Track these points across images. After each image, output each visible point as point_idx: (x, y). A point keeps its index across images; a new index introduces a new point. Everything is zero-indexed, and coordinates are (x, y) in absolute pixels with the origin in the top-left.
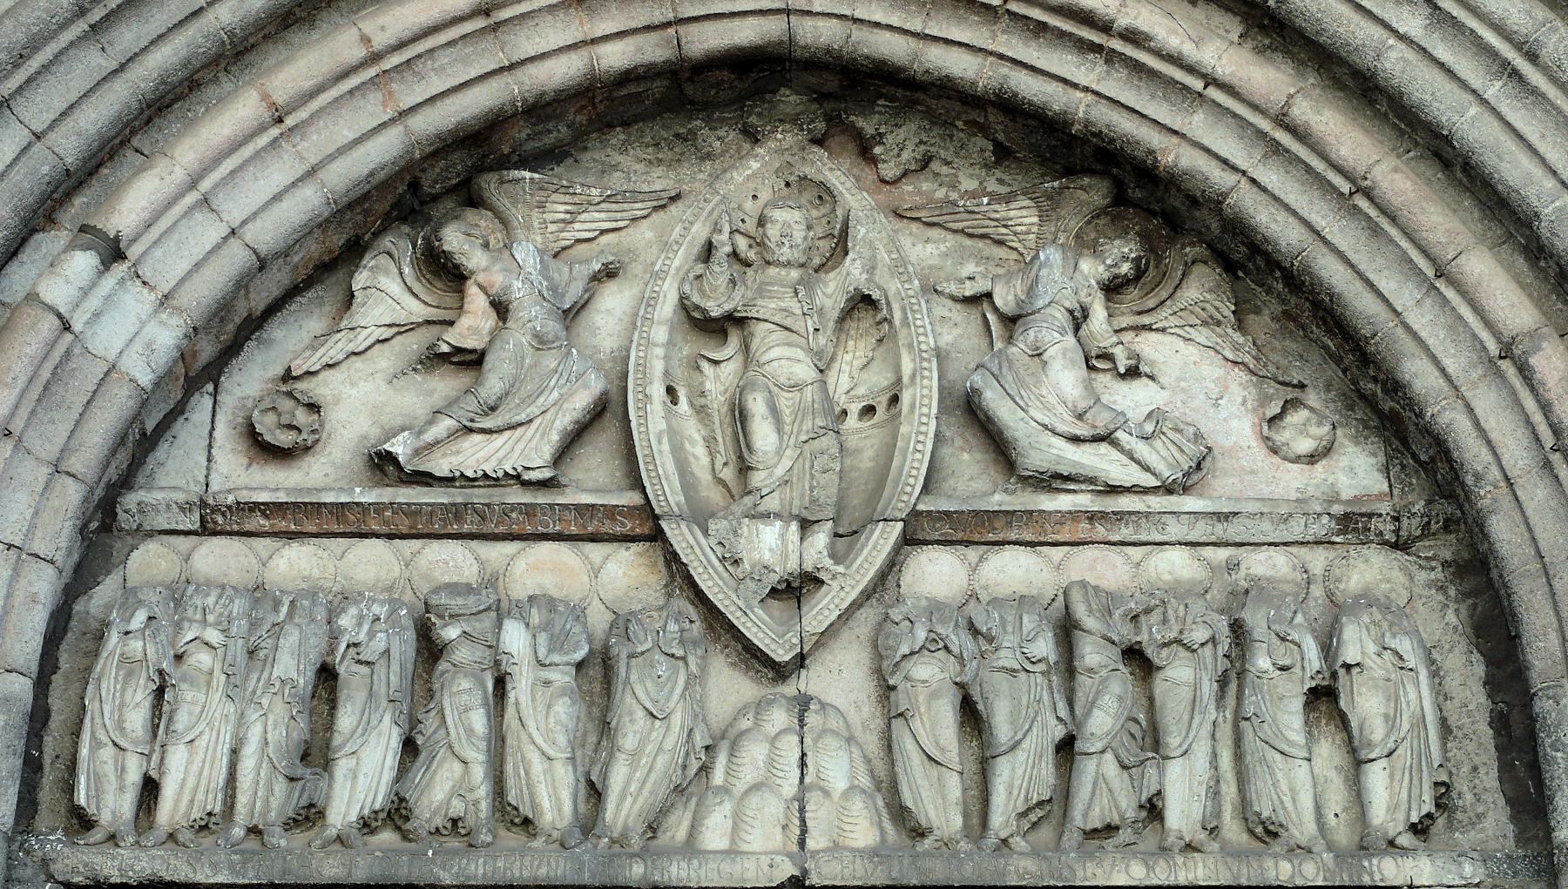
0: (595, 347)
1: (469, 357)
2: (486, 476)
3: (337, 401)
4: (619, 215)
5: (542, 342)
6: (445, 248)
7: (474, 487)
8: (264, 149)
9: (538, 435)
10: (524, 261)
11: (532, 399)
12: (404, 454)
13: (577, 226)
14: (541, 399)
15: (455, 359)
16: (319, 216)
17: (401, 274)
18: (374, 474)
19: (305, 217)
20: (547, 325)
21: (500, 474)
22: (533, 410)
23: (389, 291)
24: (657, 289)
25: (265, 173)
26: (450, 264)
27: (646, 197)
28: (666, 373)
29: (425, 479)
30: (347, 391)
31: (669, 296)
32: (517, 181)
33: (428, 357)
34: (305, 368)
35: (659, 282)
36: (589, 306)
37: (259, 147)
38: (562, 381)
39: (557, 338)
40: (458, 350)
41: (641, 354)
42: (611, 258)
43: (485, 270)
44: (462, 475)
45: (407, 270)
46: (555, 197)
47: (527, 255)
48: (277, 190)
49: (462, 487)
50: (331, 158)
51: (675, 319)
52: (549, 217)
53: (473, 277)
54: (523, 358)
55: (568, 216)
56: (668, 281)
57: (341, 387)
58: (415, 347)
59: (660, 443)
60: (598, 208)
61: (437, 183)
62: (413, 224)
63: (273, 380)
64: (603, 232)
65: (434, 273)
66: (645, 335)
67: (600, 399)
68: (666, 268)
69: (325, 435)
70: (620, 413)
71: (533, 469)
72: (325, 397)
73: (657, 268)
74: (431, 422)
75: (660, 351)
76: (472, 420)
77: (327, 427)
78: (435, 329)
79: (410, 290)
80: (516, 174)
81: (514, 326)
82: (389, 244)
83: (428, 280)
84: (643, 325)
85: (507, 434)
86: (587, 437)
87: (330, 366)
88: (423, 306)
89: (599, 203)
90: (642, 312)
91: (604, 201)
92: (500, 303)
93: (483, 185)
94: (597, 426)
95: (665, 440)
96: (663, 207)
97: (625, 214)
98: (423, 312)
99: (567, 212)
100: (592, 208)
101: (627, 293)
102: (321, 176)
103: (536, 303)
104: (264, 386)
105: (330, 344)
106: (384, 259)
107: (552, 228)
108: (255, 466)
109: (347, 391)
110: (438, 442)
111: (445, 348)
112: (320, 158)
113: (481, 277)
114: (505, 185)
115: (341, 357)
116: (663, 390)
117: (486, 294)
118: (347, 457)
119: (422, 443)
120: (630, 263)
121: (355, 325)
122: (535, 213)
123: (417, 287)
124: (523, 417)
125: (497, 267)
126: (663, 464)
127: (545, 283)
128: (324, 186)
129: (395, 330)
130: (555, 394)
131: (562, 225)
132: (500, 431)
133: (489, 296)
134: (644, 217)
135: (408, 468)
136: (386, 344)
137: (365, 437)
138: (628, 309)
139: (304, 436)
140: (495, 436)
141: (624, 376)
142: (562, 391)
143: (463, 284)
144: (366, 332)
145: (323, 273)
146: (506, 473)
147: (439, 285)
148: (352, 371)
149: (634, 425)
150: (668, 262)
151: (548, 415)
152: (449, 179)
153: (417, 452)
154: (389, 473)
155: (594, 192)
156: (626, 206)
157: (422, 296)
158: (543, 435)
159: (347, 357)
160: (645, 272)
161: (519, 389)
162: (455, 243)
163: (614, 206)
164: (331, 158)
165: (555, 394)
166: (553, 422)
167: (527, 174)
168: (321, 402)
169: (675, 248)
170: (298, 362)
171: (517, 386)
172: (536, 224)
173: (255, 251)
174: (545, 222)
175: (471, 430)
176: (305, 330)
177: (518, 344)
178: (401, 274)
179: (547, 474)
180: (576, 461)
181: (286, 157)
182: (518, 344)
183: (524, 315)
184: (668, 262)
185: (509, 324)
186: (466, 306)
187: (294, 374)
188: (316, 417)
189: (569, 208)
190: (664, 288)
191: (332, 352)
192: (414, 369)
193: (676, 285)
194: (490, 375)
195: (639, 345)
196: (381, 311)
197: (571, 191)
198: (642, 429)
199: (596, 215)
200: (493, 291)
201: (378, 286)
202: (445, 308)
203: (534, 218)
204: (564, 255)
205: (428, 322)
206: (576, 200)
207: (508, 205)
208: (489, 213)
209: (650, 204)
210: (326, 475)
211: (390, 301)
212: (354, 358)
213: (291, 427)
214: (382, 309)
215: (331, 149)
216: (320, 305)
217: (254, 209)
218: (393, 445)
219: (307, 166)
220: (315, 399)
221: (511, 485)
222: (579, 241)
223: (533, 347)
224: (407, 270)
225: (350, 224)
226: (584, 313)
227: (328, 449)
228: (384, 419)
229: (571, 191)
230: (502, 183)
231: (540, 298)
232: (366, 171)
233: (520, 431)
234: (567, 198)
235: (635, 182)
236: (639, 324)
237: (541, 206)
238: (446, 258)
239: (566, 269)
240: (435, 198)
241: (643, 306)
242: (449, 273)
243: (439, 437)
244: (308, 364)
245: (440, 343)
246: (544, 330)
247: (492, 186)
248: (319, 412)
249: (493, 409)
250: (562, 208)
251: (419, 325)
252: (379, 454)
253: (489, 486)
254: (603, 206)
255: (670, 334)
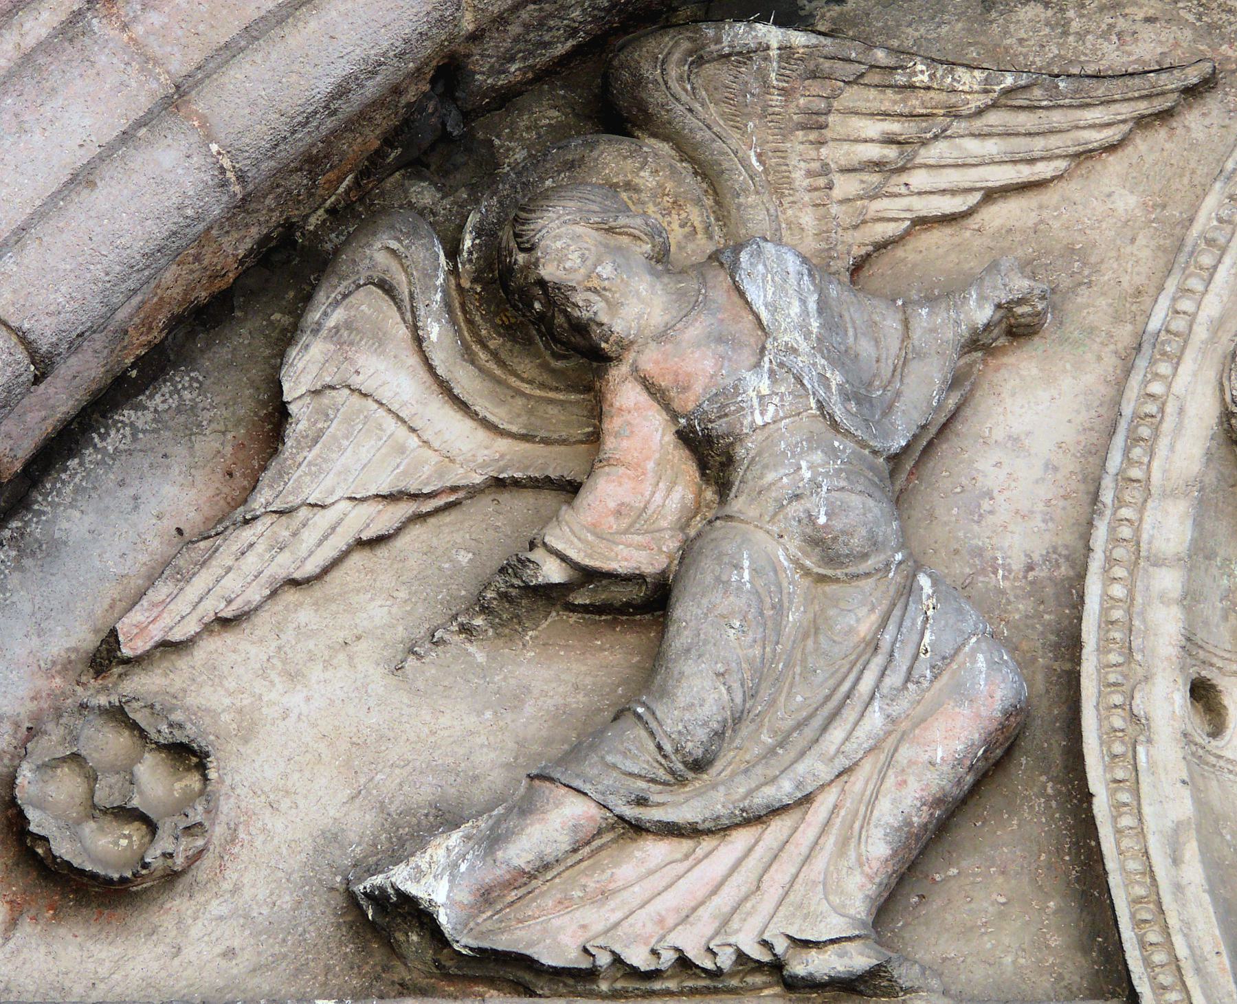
0: (979, 552)
1: (622, 594)
2: (683, 963)
3: (247, 733)
4: (1038, 144)
5: (832, 560)
6: (548, 272)
7: (652, 994)
8: (44, 46)
9: (830, 842)
10: (773, 308)
11: (809, 732)
12: (452, 904)
13: (918, 179)
14: (836, 734)
15: (580, 599)
16: (198, 218)
17: (419, 341)
18: (363, 949)
19: (157, 231)
20: (845, 508)
21: (726, 960)
22: (814, 768)
23: (385, 395)
24: (1156, 388)
25: (47, 111)
26: (560, 320)
27: (1115, 88)
28: (1190, 644)
29: (512, 973)
30: (276, 694)
31: (1192, 410)
32: (746, 55)
33: (504, 596)
34: (156, 634)
35: (1164, 368)
36: (959, 426)
37: (30, 41)
38: (894, 679)
39: (875, 544)
40: (588, 575)
41: (1118, 591)
42: (1021, 284)
43: (662, 336)
44: (617, 960)
45: (434, 330)
46: (852, 97)
47: (781, 289)
48: (83, 157)
49: (615, 994)
50: (229, 52)
51: (1211, 478)
52: (835, 154)
53: (630, 357)
54: (779, 609)
55: (891, 152)
56: (1188, 365)
57: (259, 686)
58: (464, 558)
59: (1176, 861)
60: (978, 124)
61: (512, 59)
62: (442, 177)
63: (66, 667)
64: (991, 195)
65: (510, 331)
66: (1125, 532)
67: (1003, 728)
68: (1179, 324)
69: (219, 832)
70: (1057, 757)
71: (817, 945)
72: (215, 715)
73: (1155, 324)
74: (525, 808)
75: (1169, 581)
76: (642, 801)
77: (226, 807)
78: (520, 505)
79: (445, 388)
80: (741, 34)
81: (752, 512)
82: (382, 258)
83: (495, 355)
84: (1119, 502)
85: (741, 839)
86: (964, 831)
87: (224, 623)
88: (481, 435)
89: (980, 112)
90: (1115, 461)
91: (994, 105)
92: (709, 440)
93: (650, 72)
94: (993, 799)
95: (1191, 851)
96: (1165, 116)
97: (1054, 142)
98: (483, 455)
99: (890, 140)
100: (958, 126)
101: (1066, 383)
102: (200, 107)
103: (813, 442)
104: (42, 684)
105: (224, 557)
106: (370, 304)
107: (846, 186)
108: (27, 928)
109: (276, 694)
110: (547, 867)
111: (553, 572)
112: (197, 57)
113: (650, 360)
114: (709, 69)
115: (255, 594)
116: (1180, 697)
117: (666, 405)
118: (287, 900)
119: (501, 872)
120: (1073, 290)
121: (294, 500)
122: (798, 146)
123: (465, 381)
124: (784, 790)
125: (695, 330)
126: (1187, 925)
127: (836, 378)
128: (209, 138)
129: (405, 509)
130: (875, 719)
131: (875, 178)
132: (720, 829)
133: (674, 416)
134: (1112, 148)
135: (463, 942)
136: (382, 552)
137: (332, 838)
138: (1069, 434)
139: (164, 843)
140: (707, 843)
141: (1071, 644)
142: (895, 710)
143: (601, 373)
144: (323, 520)
145: (192, 335)
146: (741, 957)
147: (526, 367)
148: (289, 635)
149: (1101, 807)
150: (1186, 305)
151: (857, 782)
152: (546, 45)
153: (486, 897)
154: (410, 952)
155: (968, 80)
156: (1057, 118)
157: (482, 406)
158: (844, 843)
159: (274, 593)
160: (1118, 319)
161: (773, 703)
162: (574, 259)
163: (1024, 120)
164: (229, 52)
165: (875, 719)
166: (872, 803)
167: (770, 34)
168: (201, 742)
169: (1207, 260)
170: (137, 616)
171: (765, 694)
172: (798, 175)
173: (23, 338)
174: (825, 170)
175: (637, 829)
176: (151, 507)
177: (766, 569)
178: (419, 341)
179: (857, 960)
180: (936, 903)
181: (102, 59)
182: (766, 569)
183: (777, 477)
184: (1186, 305)
185: (737, 505)
186: (610, 443)
187: (126, 651)
188: (193, 781)
189: (894, 127)
190: (1179, 386)
191: (231, 583)
192: (466, 630)
193: (1211, 374)
194: (688, 667)
195: (1110, 562)
196: (364, 454)
197: (900, 78)
198: (1126, 821)
199: (973, 147)
200: (687, 402)
201: (356, 381)
202: (546, 441)
203: (793, 160)
204: (880, 269)
205: (499, 484)
206: (915, 103)
207: (721, 125)
208: (665, 148)
209: (1126, 110)
210: (229, 954)
211: (390, 423)
212: (291, 596)
213: (126, 814)
214: (366, 449)
215: (229, 29)
216: (191, 431)
217: (21, 218)
218: (418, 875)
219: (159, 85)
220: (191, 730)
221: (756, 989)
222: (923, 223)
223: (807, 572)
224: (434, 330)
225: (270, 201)
226: (944, 448)
227: (232, 875)
228: (387, 782)
229: (900, 78)
230: (700, 61)
231: (821, 426)
232: (325, 86)
233: (778, 828)
234: (888, 102)
235: (1081, 36)
236: (1107, 496)
237: (814, 123)
238: (549, 302)
239: (891, 324)
240: (506, 99)
241: (1119, 440)
242: (556, 340)
243: (550, 852)
244: (167, 620)
245: (538, 555)
246: (838, 524)
247: (673, 72)
248: (202, 768)
249: (698, 766)
250: (874, 128)
251: (474, 492)
252: (378, 898)
253: (693, 992)
254: (994, 119)
255: (1198, 524)
